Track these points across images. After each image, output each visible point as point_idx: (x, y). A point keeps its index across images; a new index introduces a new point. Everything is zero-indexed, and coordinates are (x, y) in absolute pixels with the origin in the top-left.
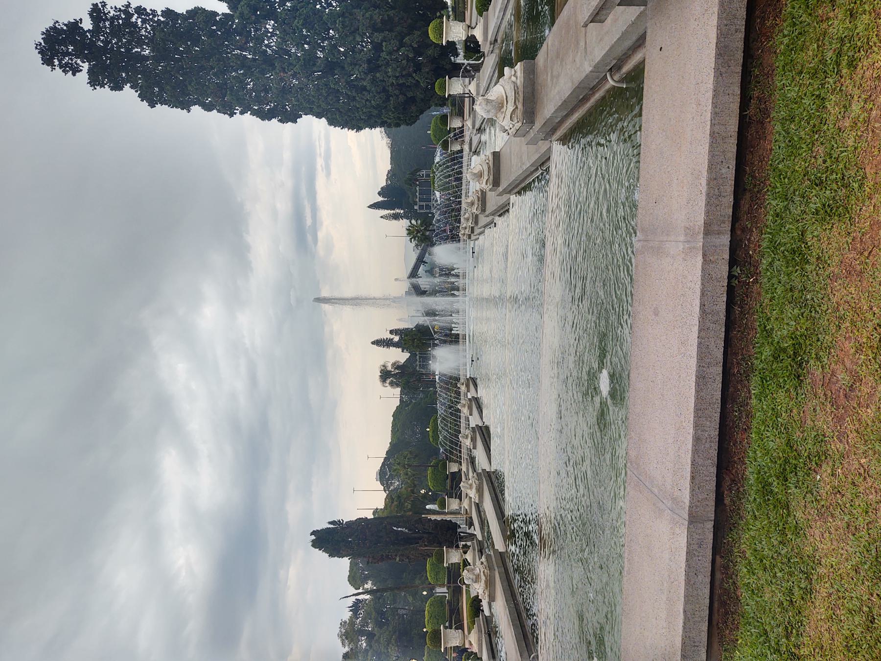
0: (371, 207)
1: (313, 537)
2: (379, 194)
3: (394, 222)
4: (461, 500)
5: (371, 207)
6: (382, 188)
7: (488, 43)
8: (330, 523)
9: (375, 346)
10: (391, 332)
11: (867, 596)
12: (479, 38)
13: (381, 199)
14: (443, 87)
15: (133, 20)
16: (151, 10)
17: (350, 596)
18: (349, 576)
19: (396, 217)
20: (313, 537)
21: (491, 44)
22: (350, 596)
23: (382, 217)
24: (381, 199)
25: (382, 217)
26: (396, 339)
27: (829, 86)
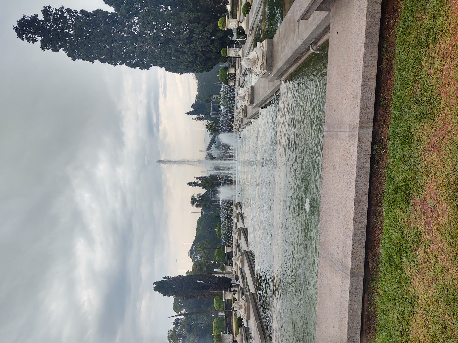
0: (187, 113)
1: (155, 285)
2: (192, 107)
3: (199, 121)
5: (187, 113)
6: (193, 104)
8: (164, 278)
9: (188, 186)
10: (197, 178)
13: (192, 109)
15: (65, 15)
16: (74, 10)
17: (174, 316)
19: (200, 119)
20: (155, 285)
22: (174, 316)
23: (193, 119)
24: (192, 109)
25: (193, 119)
26: (200, 182)
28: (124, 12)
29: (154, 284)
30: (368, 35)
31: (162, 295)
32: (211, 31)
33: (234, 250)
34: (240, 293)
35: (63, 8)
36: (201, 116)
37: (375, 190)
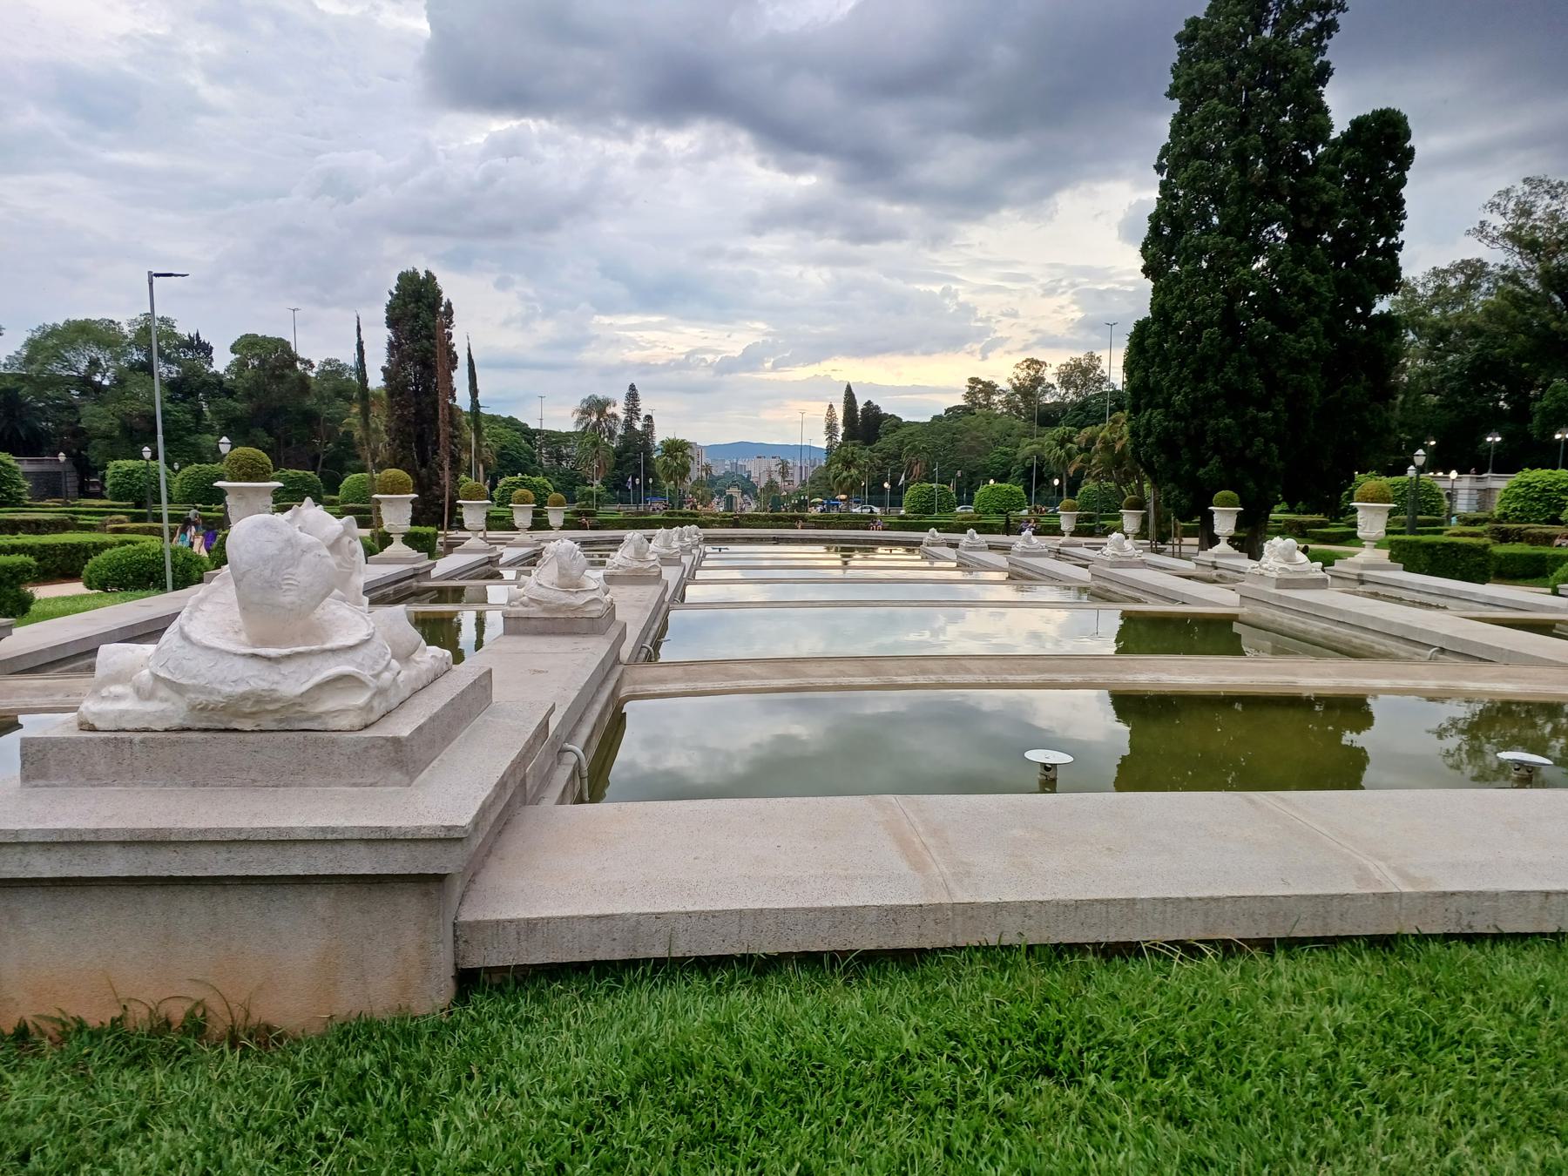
0: (849, 389)
1: (422, 275)
2: (869, 403)
3: (823, 428)
4: (530, 529)
5: (849, 389)
6: (877, 408)
7: (1358, 572)
8: (449, 305)
9: (627, 390)
10: (649, 418)
11: (430, 1083)
12: (1216, 549)
13: (860, 406)
14: (1227, 503)
15: (1315, 16)
16: (1326, 47)
17: (359, 335)
18: (255, 336)
19: (831, 428)
20: (422, 275)
21: (1359, 575)
22: (359, 335)
23: (831, 406)
24: (860, 406)
25: (831, 406)
26: (638, 426)
27: (1506, 988)
28: (1325, 197)
29: (427, 272)
30: (61, 831)
31: (1142, 262)
32: (1261, 462)
33: (519, 537)
34: (415, 566)
35: (1341, 8)
36: (841, 430)
37: (539, 998)
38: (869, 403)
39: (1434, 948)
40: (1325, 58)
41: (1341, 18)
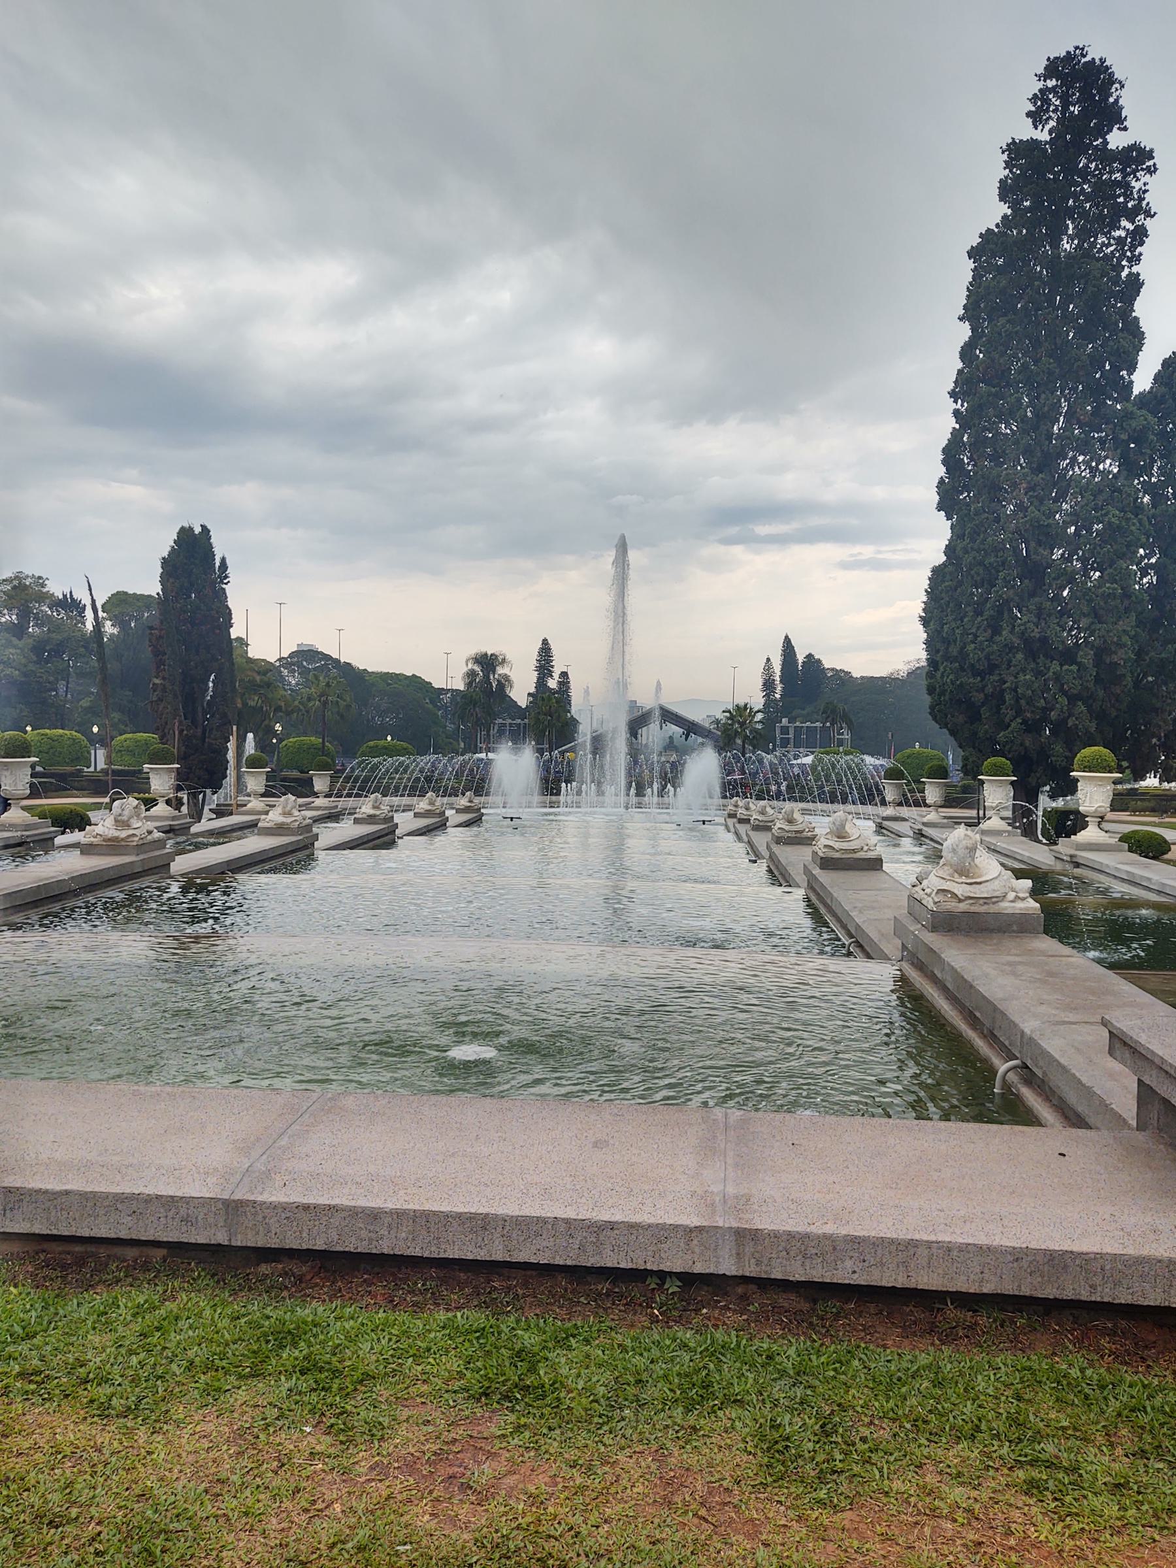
0: (787, 640)
1: (198, 530)
2: (810, 656)
3: (759, 682)
4: (263, 795)
5: (787, 640)
6: (819, 661)
7: (1073, 852)
9: (539, 645)
10: (564, 675)
13: (801, 658)
14: (997, 771)
15: (1124, 223)
16: (1141, 254)
17: (91, 594)
18: (125, 593)
19: (768, 685)
20: (198, 530)
21: (1071, 856)
22: (91, 594)
23: (768, 660)
24: (801, 658)
25: (768, 660)
28: (1134, 424)
36: (779, 688)
37: (525, 1285)
38: (810, 656)
39: (952, 1312)
40: (1135, 269)
41: (1149, 223)
